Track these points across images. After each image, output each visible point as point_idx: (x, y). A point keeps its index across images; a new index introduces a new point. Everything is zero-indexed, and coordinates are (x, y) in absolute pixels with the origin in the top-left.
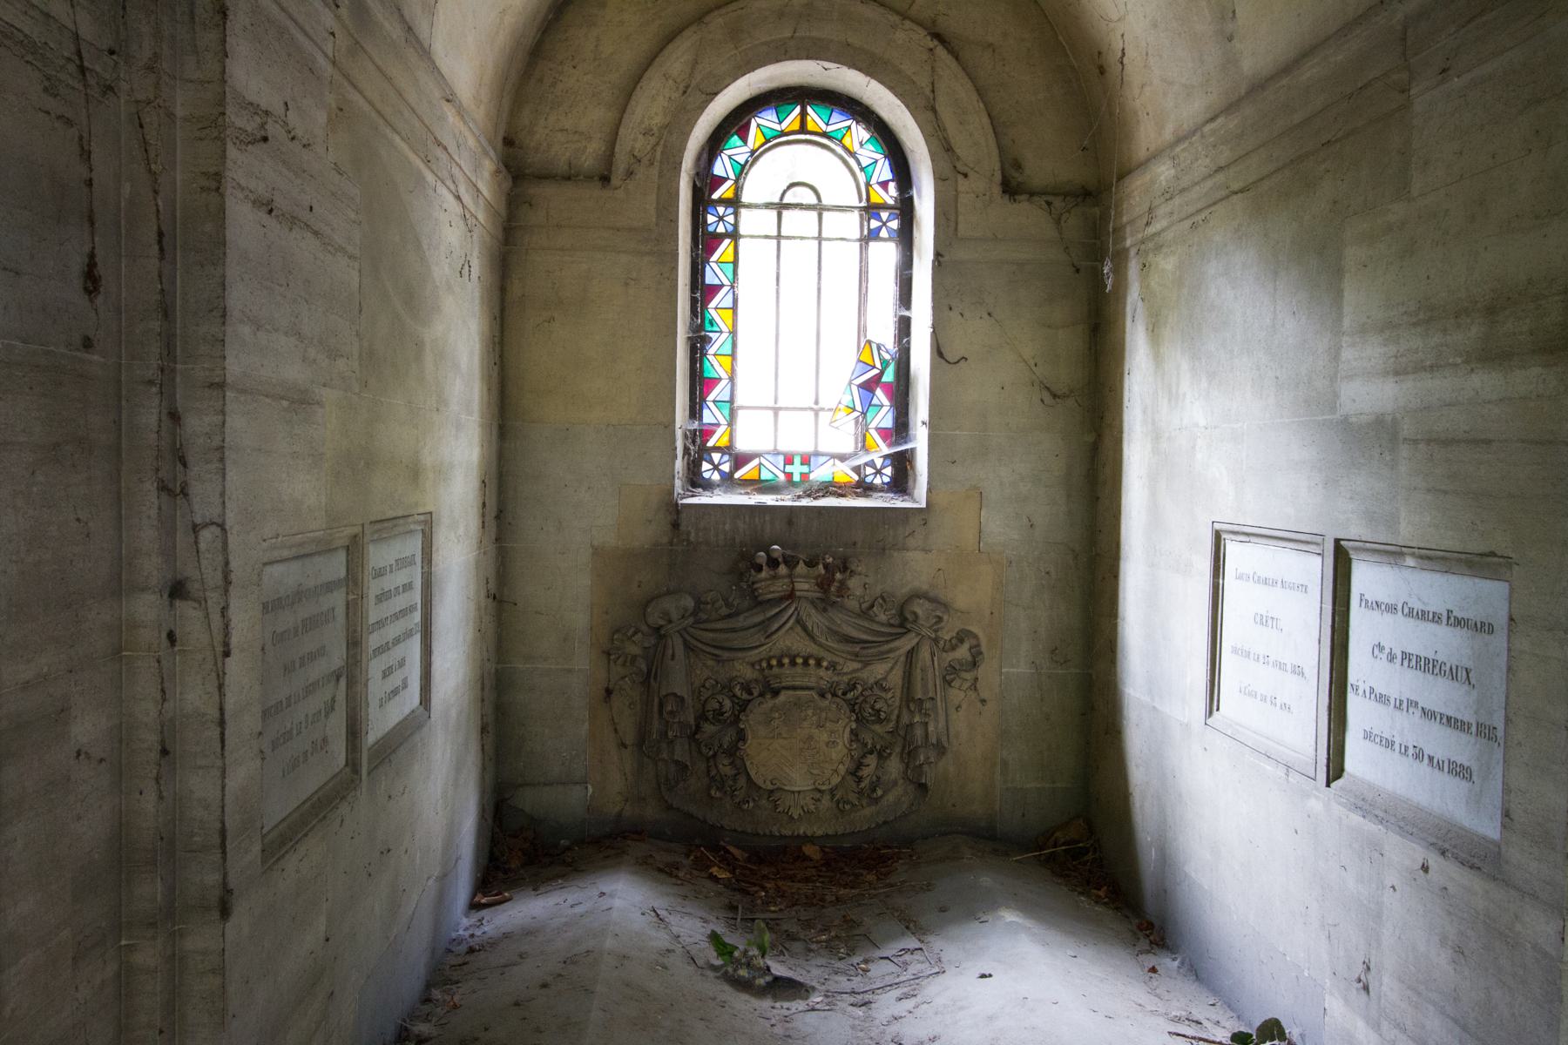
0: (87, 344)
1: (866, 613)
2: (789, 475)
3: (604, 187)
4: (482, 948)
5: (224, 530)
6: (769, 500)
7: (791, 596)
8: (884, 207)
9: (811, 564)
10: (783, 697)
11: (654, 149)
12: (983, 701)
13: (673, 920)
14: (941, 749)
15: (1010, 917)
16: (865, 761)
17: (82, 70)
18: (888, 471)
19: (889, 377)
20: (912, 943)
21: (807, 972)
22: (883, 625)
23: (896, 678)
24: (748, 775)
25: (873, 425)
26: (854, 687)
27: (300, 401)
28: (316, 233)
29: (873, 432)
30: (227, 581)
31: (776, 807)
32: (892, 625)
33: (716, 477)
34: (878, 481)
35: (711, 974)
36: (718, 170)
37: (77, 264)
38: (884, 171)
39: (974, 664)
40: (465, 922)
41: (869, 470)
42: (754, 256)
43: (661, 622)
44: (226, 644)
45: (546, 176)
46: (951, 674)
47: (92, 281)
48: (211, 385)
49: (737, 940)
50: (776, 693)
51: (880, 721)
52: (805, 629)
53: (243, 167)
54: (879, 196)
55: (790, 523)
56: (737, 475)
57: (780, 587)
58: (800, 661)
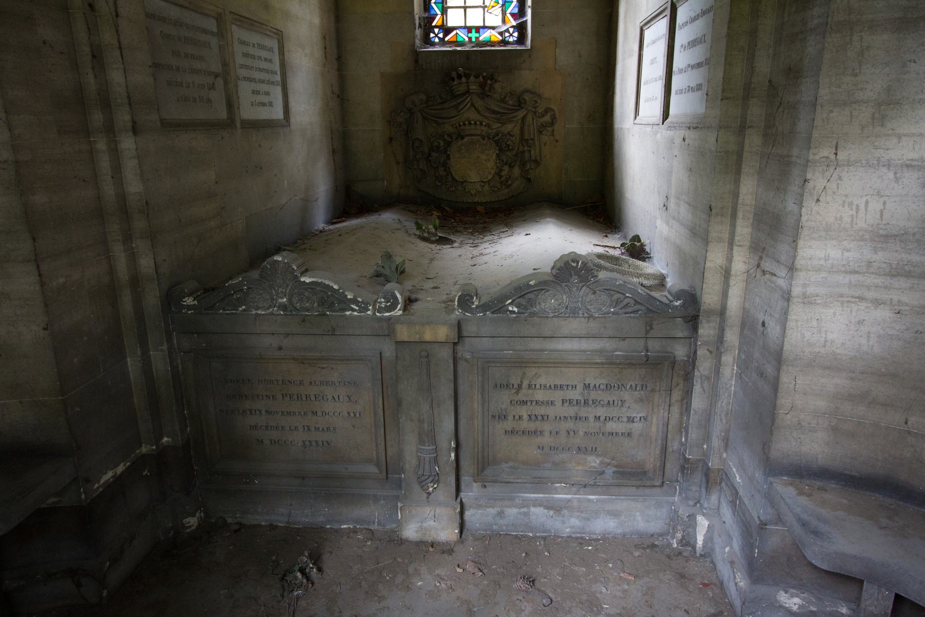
1: (503, 101)
2: (470, 38)
7: (468, 92)
9: (477, 77)
10: (466, 139)
12: (557, 141)
13: (406, 223)
14: (537, 163)
18: (516, 34)
21: (452, 237)
23: (517, 131)
29: (509, 15)
33: (437, 40)
34: (511, 39)
39: (552, 124)
41: (507, 34)
50: (463, 138)
51: (510, 150)
52: (475, 108)
55: (468, 58)
56: (446, 39)
57: (463, 89)
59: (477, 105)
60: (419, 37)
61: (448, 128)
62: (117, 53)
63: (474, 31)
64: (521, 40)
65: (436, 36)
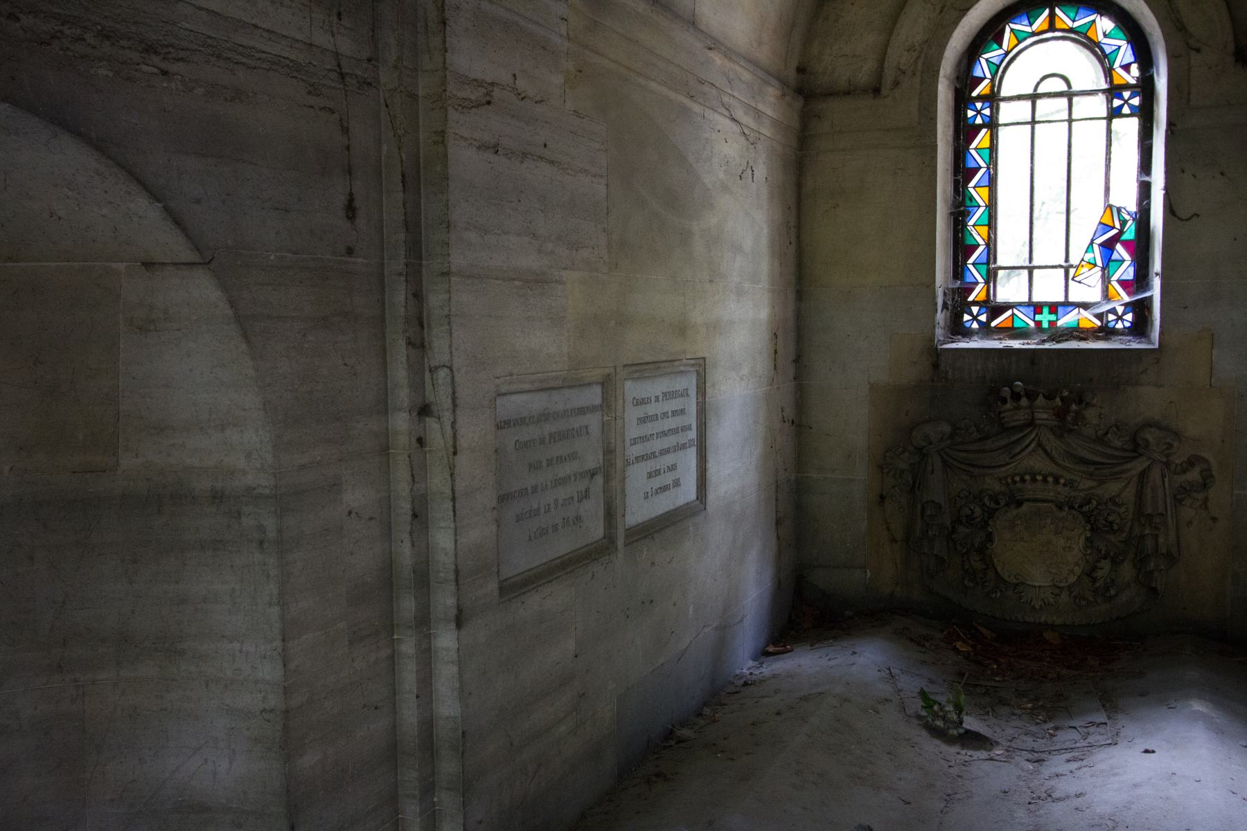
0: (350, 251)
1: (1101, 440)
2: (1038, 323)
3: (875, 97)
4: (753, 683)
5: (451, 370)
6: (1016, 344)
7: (1031, 424)
8: (1127, 86)
9: (1049, 397)
10: (1025, 507)
11: (916, 62)
12: (1214, 519)
15: (1198, 706)
16: (1099, 565)
17: (342, 76)
18: (1129, 317)
19: (1130, 234)
20: (1101, 717)
22: (1116, 449)
23: (1129, 495)
24: (996, 572)
25: (1115, 277)
26: (1089, 502)
27: (538, 281)
28: (552, 162)
30: (455, 405)
31: (1020, 598)
32: (1126, 450)
33: (975, 325)
34: (1119, 326)
35: (916, 722)
36: (978, 73)
37: (340, 201)
38: (1125, 54)
39: (1205, 486)
40: (751, 663)
41: (1111, 317)
42: (1012, 142)
43: (924, 444)
44: (455, 447)
45: (831, 93)
46: (1180, 495)
47: (351, 210)
48: (443, 274)
49: (943, 697)
50: (1019, 504)
51: (1114, 532)
52: (1045, 451)
53: (460, 124)
54: (1122, 77)
56: (993, 324)
57: (1022, 417)
58: (1039, 478)
59: (1048, 448)
60: (942, 323)
61: (992, 484)
62: (449, 505)
63: (1046, 310)
64: (1140, 327)
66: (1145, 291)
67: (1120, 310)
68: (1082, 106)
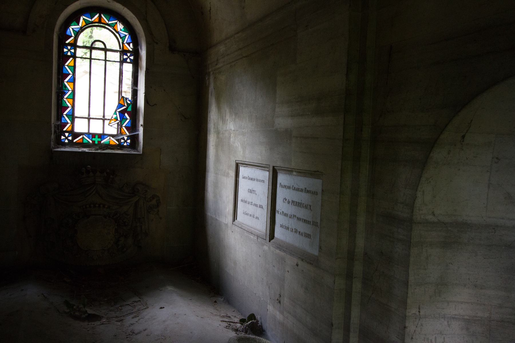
2: (94, 142)
6: (86, 150)
8: (129, 51)
12: (161, 218)
15: (170, 288)
18: (129, 141)
19: (129, 109)
20: (137, 299)
33: (66, 141)
38: (127, 39)
41: (122, 141)
42: (82, 66)
56: (75, 141)
63: (97, 136)
65: (66, 138)
66: (135, 132)
67: (126, 138)
68: (110, 55)
